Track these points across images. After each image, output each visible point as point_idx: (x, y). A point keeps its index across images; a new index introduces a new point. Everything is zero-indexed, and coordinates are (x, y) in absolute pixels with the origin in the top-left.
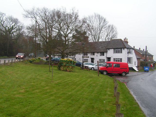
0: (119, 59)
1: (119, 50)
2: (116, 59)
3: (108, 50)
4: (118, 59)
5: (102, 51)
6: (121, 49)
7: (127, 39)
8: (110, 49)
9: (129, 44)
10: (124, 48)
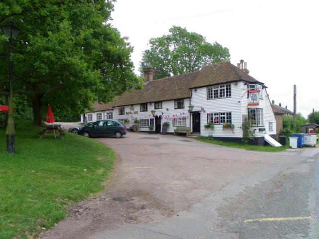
0: (224, 114)
1: (222, 88)
3: (194, 93)
4: (221, 114)
5: (179, 96)
6: (228, 84)
7: (246, 63)
8: (198, 90)
9: (249, 74)
10: (236, 82)
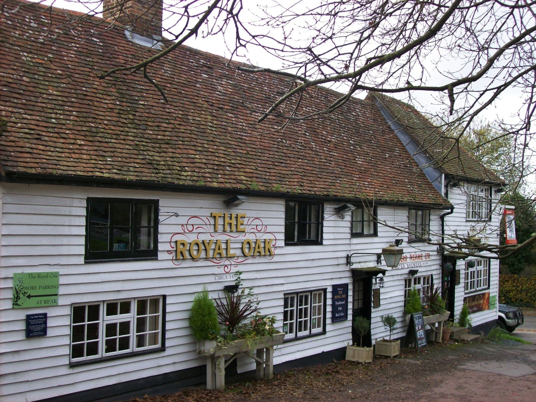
0: (125, 307)
2: (105, 320)
